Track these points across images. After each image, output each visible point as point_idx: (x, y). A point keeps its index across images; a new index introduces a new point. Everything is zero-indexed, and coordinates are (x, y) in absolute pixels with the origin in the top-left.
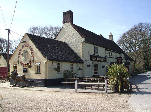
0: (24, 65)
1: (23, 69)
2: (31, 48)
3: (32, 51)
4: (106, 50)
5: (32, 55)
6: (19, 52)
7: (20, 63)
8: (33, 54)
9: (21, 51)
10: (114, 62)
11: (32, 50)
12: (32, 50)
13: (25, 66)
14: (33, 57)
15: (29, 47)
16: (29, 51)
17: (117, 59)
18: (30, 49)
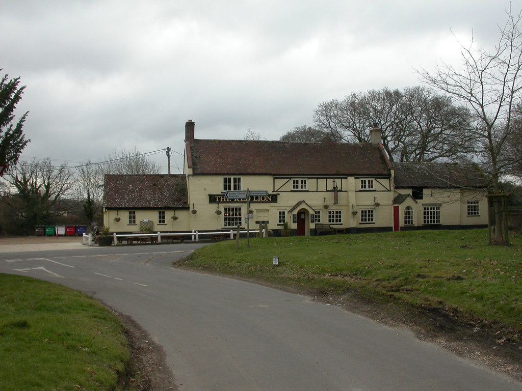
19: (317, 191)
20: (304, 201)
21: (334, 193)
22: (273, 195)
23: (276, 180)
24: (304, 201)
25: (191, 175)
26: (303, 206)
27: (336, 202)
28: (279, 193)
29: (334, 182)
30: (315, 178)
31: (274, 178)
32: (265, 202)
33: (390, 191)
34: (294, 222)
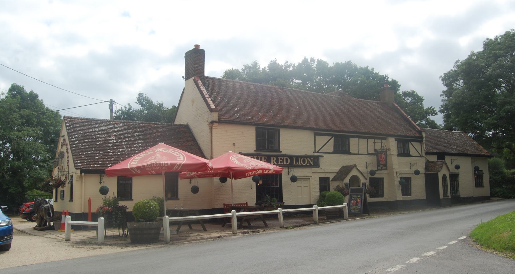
4: (316, 134)
17: (375, 157)
19: (359, 154)
20: (355, 166)
21: (375, 157)
22: (314, 157)
23: (317, 137)
24: (355, 166)
25: (216, 122)
26: (354, 172)
27: (71, 200)
28: (323, 154)
29: (375, 143)
30: (287, 167)
31: (316, 134)
32: (306, 166)
33: (421, 156)
34: (62, 154)
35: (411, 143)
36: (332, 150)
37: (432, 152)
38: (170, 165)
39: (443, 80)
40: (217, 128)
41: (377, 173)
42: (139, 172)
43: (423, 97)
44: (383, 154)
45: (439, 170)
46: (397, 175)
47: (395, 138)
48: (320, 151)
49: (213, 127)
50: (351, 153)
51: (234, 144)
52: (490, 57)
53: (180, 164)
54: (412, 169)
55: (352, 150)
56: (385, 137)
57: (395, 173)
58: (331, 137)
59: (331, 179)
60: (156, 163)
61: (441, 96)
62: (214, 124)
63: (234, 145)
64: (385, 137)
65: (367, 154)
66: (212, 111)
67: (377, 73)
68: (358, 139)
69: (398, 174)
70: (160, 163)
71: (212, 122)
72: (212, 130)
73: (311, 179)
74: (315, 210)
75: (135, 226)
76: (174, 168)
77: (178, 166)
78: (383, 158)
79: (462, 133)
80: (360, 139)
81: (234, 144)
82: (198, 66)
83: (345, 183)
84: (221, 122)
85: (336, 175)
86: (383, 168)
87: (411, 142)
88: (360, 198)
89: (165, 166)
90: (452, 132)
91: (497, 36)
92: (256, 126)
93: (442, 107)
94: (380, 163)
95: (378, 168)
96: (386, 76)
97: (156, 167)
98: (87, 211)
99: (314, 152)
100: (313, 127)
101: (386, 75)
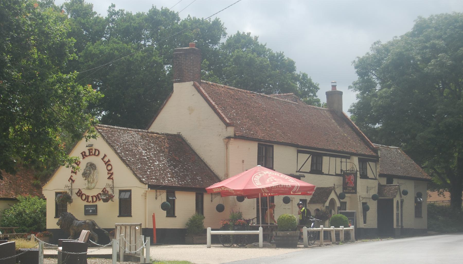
0: (87, 197)
1: (86, 206)
2: (106, 159)
3: (109, 168)
4: (299, 152)
5: (110, 175)
6: (76, 173)
7: (77, 194)
8: (112, 174)
9: (78, 165)
10: (356, 190)
11: (108, 164)
12: (108, 164)
13: (90, 199)
14: (111, 180)
15: (102, 156)
16: (102, 168)
17: (341, 178)
18: (104, 162)
19: (329, 175)
21: (341, 178)
23: (299, 154)
28: (305, 174)
29: (341, 162)
31: (299, 152)
35: (310, 156)
36: (309, 170)
37: (383, 174)
38: (291, 187)
39: (356, 67)
40: (232, 143)
41: (347, 197)
42: (267, 191)
43: (318, 85)
44: (353, 175)
45: (394, 196)
46: (360, 200)
47: (358, 158)
48: (301, 170)
49: (230, 143)
50: (323, 173)
51: (243, 161)
52: (426, 47)
53: (298, 186)
54: (368, 193)
55: (325, 170)
56: (349, 155)
57: (358, 197)
58: (310, 155)
59: (308, 202)
60: (281, 185)
61: (349, 89)
62: (232, 139)
63: (243, 162)
64: (349, 155)
65: (335, 174)
66: (227, 125)
67: (263, 44)
68: (345, 159)
69: (361, 199)
70: (284, 185)
71: (229, 138)
72: (228, 145)
73: (293, 200)
74: (342, 230)
75: (288, 233)
76: (294, 189)
77: (296, 188)
78: (352, 180)
79: (398, 149)
80: (331, 158)
81: (243, 161)
82: (196, 69)
83: (326, 206)
84: (236, 137)
85: (312, 197)
86: (351, 191)
87: (369, 162)
88: (351, 222)
89: (287, 188)
90: (389, 147)
91: (432, 16)
92: (259, 142)
93: (354, 106)
94: (348, 185)
95: (344, 191)
96: (280, 53)
97: (280, 188)
98: (151, 227)
99: (297, 172)
100: (298, 144)
101: (282, 52)
